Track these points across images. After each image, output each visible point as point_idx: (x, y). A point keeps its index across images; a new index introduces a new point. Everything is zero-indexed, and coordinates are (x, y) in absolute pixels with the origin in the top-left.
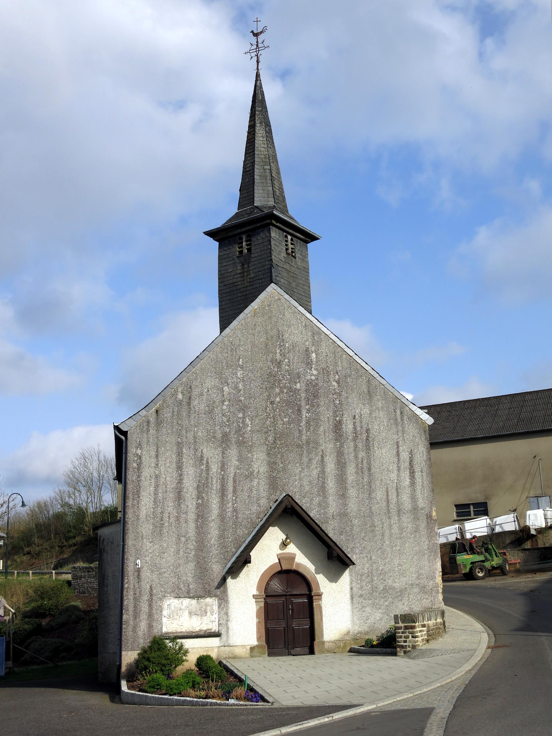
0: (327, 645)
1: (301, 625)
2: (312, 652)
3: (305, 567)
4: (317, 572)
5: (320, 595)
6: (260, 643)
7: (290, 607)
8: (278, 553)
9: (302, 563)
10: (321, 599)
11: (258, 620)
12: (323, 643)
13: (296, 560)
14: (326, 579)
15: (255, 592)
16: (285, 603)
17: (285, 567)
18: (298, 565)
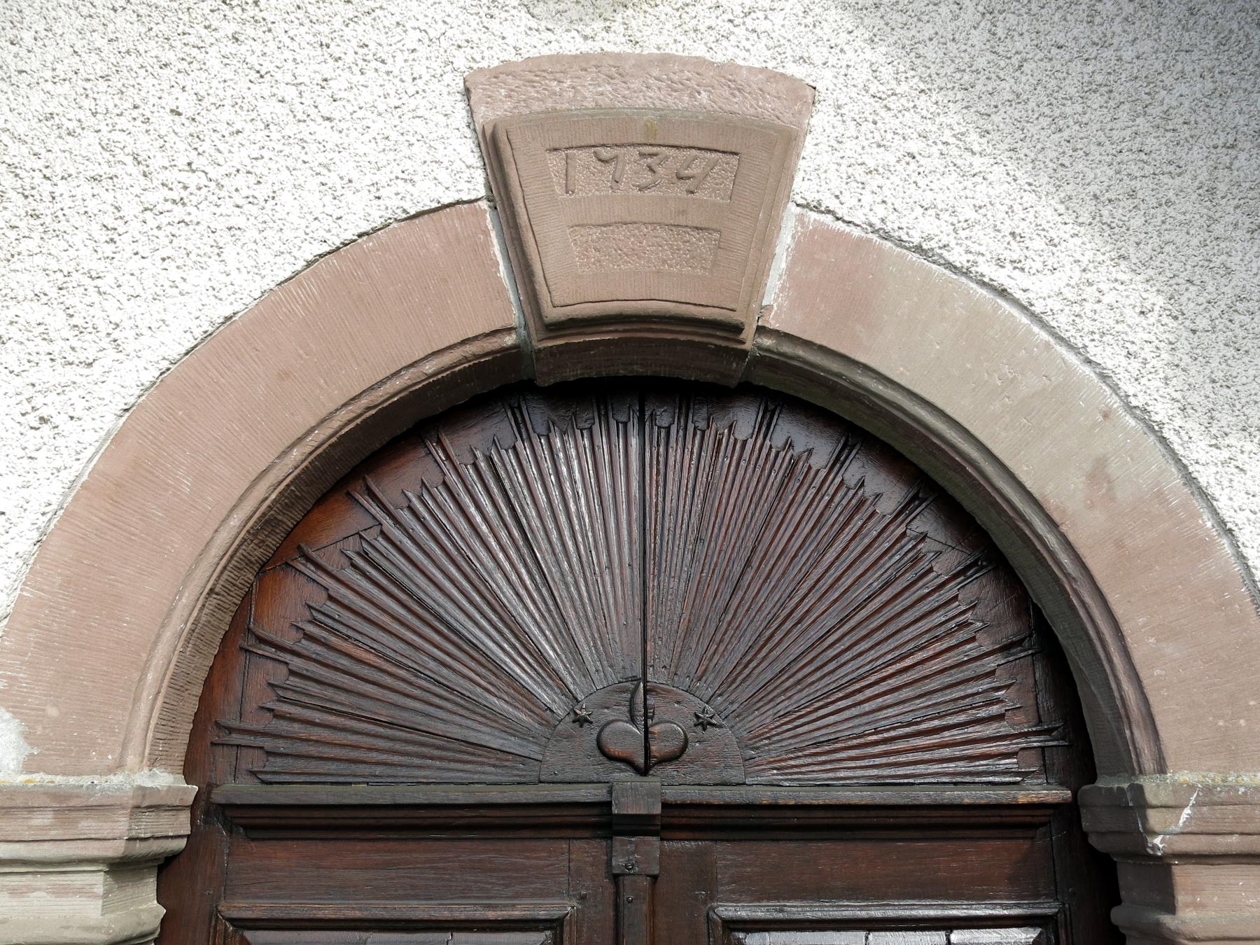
13: (803, 187)
17: (603, 265)
18: (848, 259)
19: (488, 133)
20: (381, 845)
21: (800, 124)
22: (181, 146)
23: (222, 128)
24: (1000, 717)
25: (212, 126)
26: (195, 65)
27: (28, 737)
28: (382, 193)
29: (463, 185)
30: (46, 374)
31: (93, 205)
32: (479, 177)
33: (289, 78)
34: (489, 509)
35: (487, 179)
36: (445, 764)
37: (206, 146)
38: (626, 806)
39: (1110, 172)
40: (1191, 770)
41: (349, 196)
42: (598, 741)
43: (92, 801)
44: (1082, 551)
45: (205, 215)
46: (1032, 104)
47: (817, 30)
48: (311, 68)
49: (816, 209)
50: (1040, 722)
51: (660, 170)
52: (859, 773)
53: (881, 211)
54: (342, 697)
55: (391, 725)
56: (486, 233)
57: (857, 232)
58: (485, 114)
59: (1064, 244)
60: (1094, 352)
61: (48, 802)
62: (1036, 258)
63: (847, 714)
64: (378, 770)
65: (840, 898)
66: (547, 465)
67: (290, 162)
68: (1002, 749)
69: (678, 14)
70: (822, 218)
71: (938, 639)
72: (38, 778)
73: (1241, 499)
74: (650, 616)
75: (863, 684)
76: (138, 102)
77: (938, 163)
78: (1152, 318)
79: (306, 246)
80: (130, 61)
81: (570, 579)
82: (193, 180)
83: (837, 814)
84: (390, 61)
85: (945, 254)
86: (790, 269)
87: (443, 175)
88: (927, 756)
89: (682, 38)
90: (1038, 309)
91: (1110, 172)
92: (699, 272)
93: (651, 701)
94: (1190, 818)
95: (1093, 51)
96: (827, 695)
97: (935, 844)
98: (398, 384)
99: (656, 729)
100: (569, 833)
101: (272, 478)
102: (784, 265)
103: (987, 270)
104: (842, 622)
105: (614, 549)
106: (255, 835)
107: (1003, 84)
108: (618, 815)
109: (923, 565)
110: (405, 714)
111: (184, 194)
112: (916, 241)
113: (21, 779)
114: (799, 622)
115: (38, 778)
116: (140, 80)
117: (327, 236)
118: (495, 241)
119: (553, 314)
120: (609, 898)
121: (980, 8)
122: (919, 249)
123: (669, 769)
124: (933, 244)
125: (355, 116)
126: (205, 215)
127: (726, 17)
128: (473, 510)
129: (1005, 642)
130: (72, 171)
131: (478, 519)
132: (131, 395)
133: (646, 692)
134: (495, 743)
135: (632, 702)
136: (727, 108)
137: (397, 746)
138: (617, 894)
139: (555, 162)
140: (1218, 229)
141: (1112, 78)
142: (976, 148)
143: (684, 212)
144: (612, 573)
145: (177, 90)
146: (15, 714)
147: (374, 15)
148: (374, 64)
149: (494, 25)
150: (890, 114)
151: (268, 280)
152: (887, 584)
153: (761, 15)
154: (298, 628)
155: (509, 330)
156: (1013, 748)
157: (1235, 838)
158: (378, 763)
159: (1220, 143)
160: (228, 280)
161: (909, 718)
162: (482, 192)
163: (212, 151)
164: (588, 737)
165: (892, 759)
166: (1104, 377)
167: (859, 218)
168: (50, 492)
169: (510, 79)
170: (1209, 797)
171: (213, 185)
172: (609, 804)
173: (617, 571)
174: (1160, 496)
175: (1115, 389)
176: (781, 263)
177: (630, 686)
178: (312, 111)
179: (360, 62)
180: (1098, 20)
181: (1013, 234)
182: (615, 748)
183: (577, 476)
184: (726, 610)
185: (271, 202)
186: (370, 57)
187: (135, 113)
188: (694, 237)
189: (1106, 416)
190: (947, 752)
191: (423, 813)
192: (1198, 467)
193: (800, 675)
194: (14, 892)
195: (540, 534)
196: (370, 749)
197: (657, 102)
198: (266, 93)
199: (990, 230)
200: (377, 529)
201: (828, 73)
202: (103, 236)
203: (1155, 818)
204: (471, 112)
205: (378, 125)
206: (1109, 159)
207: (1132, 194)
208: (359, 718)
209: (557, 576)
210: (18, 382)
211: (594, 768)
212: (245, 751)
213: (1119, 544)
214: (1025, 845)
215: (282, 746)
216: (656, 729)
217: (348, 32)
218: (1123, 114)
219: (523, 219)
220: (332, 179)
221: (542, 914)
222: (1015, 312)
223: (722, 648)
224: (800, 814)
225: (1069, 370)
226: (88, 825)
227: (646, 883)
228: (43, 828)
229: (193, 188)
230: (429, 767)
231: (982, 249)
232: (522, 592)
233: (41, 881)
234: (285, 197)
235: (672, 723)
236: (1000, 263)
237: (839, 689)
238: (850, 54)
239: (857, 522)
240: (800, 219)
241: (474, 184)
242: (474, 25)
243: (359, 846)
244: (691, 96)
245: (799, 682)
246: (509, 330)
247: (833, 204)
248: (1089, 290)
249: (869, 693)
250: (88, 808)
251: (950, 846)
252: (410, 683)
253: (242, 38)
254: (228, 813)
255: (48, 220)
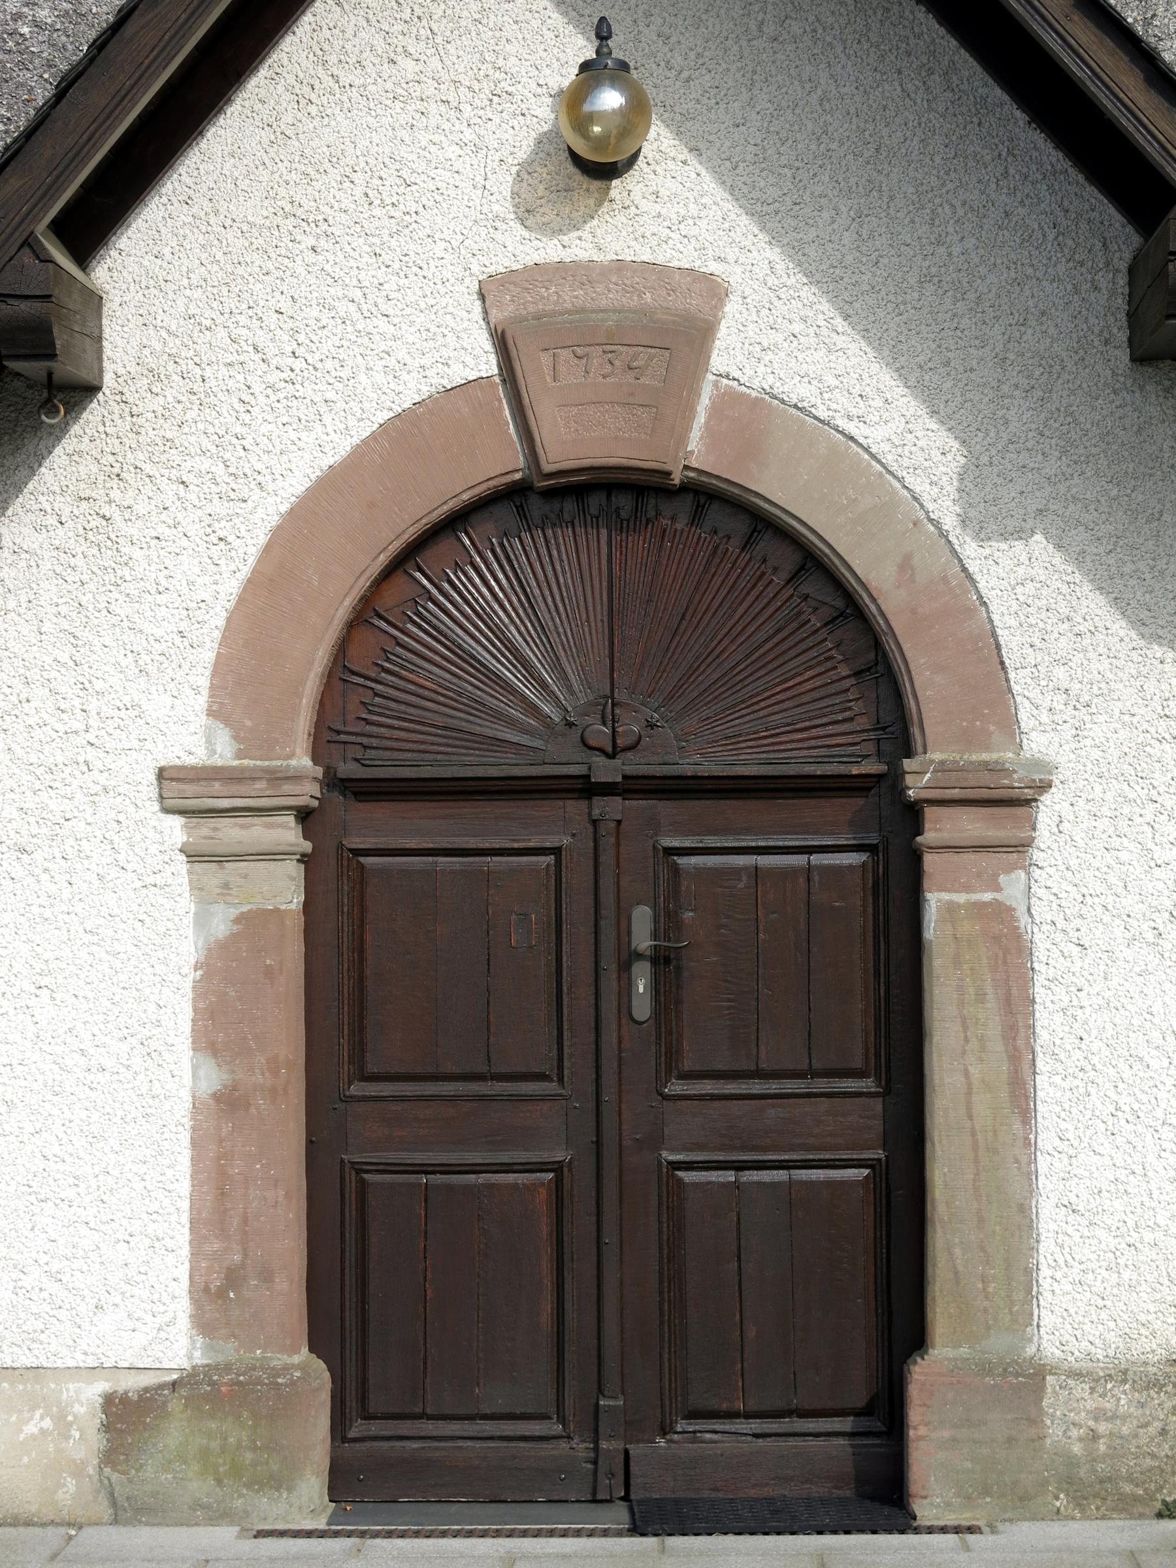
0: (1067, 1417)
1: (753, 1152)
2: (881, 1495)
3: (842, 455)
4: (989, 521)
5: (1010, 800)
6: (229, 1351)
7: (642, 920)
8: (500, 263)
9: (797, 391)
10: (1022, 847)
11: (213, 1078)
12: (1028, 1380)
13: (719, 361)
14: (1094, 605)
15: (190, 733)
16: (578, 878)
17: (577, 437)
18: (748, 414)
19: (499, 332)
20: (443, 804)
21: (715, 316)
22: (286, 338)
23: (312, 322)
24: (851, 719)
25: (305, 321)
26: (288, 273)
27: (236, 738)
28: (428, 373)
29: (483, 367)
30: (219, 508)
31: (231, 383)
32: (493, 359)
33: (355, 282)
34: (504, 581)
35: (498, 361)
36: (482, 753)
37: (301, 338)
38: (599, 777)
39: (933, 346)
40: (941, 752)
41: (404, 376)
42: (582, 737)
43: (289, 774)
44: (889, 617)
45: (307, 391)
46: (883, 293)
47: (732, 234)
48: (370, 273)
49: (727, 377)
50: (878, 722)
51: (617, 363)
52: (754, 756)
53: (771, 379)
54: (411, 710)
55: (445, 728)
56: (500, 401)
57: (754, 394)
58: (496, 315)
59: (896, 402)
60: (909, 480)
61: (263, 775)
62: (876, 413)
63: (748, 718)
64: (439, 757)
65: (739, 834)
66: (543, 551)
67: (362, 350)
68: (850, 741)
69: (631, 223)
70: (731, 383)
71: (811, 668)
72: (246, 762)
73: (994, 582)
74: (617, 655)
75: (759, 698)
76: (251, 304)
77: (813, 340)
78: (950, 457)
79: (378, 413)
80: (240, 270)
81: (561, 630)
82: (298, 364)
83: (736, 782)
84: (425, 267)
85: (813, 410)
86: (707, 422)
87: (469, 360)
88: (800, 745)
89: (633, 243)
90: (873, 450)
91: (933, 346)
92: (643, 436)
93: (617, 711)
94: (930, 779)
95: (930, 249)
96: (734, 706)
97: (802, 801)
98: (445, 508)
99: (620, 729)
100: (564, 795)
101: (367, 574)
102: (703, 421)
103: (841, 423)
104: (747, 657)
105: (591, 608)
106: (362, 798)
107: (864, 277)
108: (596, 783)
109: (804, 617)
110: (455, 721)
111: (293, 375)
112: (795, 401)
113: (236, 763)
114: (718, 657)
115: (246, 762)
116: (251, 286)
117: (393, 406)
118: (506, 407)
119: (547, 468)
120: (591, 836)
121: (852, 213)
122: (796, 406)
123: (629, 755)
124: (805, 404)
125: (404, 312)
126: (307, 391)
127: (665, 224)
128: (493, 583)
129: (858, 669)
130: (214, 359)
131: (497, 589)
132: (275, 520)
133: (613, 705)
134: (515, 739)
135: (603, 711)
136: (665, 304)
137: (450, 741)
138: (595, 832)
139: (545, 359)
140: (1005, 388)
141: (943, 270)
142: (840, 330)
143: (632, 394)
144: (589, 626)
145: (277, 294)
146: (226, 725)
147: (411, 228)
148: (415, 269)
149: (498, 235)
150: (781, 302)
151: (354, 439)
152: (779, 631)
153: (691, 222)
154: (377, 664)
155: (517, 471)
156: (859, 740)
157: (957, 790)
158: (438, 753)
159: (1014, 322)
160: (328, 439)
161: (789, 720)
162: (496, 371)
163: (308, 342)
164: (575, 735)
165: (776, 748)
166: (916, 499)
167: (756, 384)
168: (232, 586)
169: (512, 287)
170: (942, 767)
171: (311, 368)
172: (588, 777)
173: (593, 624)
174: (945, 580)
175: (922, 506)
176: (701, 418)
177: (602, 701)
178: (374, 310)
179: (404, 269)
180: (937, 222)
181: (861, 396)
182: (592, 743)
183: (564, 557)
184: (667, 650)
185: (352, 381)
186: (411, 264)
187: (250, 312)
188: (640, 411)
189: (915, 524)
190: (813, 743)
191: (471, 783)
192: (969, 561)
193: (717, 693)
194: (242, 827)
195: (540, 599)
196: (432, 744)
197: (615, 302)
198: (340, 294)
199: (845, 393)
200: (427, 595)
201: (738, 270)
202: (241, 408)
203: (909, 780)
204: (485, 312)
205: (420, 319)
206: (933, 336)
207: (947, 363)
208: (423, 724)
209: (552, 628)
210: (199, 512)
211: (580, 755)
212: (349, 746)
213: (914, 611)
214: (861, 801)
215: (375, 742)
216: (620, 729)
217: (393, 243)
218: (948, 300)
219: (526, 401)
220: (391, 362)
221: (548, 845)
222: (860, 451)
223: (665, 675)
224: (712, 782)
225: (894, 492)
226: (287, 788)
227: (613, 825)
228: (261, 789)
229: (297, 371)
230: (471, 755)
231: (835, 407)
232: (529, 639)
233: (257, 820)
234: (362, 377)
235: (631, 727)
236: (850, 418)
237: (743, 702)
238: (755, 253)
239: (760, 587)
240: (716, 384)
241: (488, 365)
242: (483, 234)
243: (428, 804)
244: (639, 296)
245: (716, 698)
246: (517, 471)
247: (736, 374)
248: (909, 436)
249: (763, 704)
250: (287, 778)
251: (812, 802)
252: (456, 701)
253: (319, 250)
254: (347, 784)
255: (202, 396)
